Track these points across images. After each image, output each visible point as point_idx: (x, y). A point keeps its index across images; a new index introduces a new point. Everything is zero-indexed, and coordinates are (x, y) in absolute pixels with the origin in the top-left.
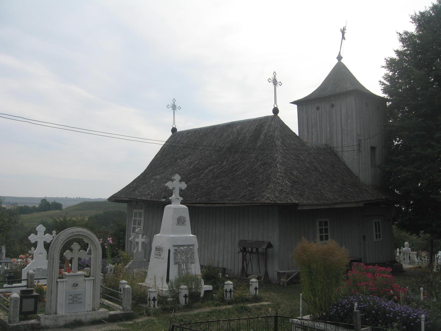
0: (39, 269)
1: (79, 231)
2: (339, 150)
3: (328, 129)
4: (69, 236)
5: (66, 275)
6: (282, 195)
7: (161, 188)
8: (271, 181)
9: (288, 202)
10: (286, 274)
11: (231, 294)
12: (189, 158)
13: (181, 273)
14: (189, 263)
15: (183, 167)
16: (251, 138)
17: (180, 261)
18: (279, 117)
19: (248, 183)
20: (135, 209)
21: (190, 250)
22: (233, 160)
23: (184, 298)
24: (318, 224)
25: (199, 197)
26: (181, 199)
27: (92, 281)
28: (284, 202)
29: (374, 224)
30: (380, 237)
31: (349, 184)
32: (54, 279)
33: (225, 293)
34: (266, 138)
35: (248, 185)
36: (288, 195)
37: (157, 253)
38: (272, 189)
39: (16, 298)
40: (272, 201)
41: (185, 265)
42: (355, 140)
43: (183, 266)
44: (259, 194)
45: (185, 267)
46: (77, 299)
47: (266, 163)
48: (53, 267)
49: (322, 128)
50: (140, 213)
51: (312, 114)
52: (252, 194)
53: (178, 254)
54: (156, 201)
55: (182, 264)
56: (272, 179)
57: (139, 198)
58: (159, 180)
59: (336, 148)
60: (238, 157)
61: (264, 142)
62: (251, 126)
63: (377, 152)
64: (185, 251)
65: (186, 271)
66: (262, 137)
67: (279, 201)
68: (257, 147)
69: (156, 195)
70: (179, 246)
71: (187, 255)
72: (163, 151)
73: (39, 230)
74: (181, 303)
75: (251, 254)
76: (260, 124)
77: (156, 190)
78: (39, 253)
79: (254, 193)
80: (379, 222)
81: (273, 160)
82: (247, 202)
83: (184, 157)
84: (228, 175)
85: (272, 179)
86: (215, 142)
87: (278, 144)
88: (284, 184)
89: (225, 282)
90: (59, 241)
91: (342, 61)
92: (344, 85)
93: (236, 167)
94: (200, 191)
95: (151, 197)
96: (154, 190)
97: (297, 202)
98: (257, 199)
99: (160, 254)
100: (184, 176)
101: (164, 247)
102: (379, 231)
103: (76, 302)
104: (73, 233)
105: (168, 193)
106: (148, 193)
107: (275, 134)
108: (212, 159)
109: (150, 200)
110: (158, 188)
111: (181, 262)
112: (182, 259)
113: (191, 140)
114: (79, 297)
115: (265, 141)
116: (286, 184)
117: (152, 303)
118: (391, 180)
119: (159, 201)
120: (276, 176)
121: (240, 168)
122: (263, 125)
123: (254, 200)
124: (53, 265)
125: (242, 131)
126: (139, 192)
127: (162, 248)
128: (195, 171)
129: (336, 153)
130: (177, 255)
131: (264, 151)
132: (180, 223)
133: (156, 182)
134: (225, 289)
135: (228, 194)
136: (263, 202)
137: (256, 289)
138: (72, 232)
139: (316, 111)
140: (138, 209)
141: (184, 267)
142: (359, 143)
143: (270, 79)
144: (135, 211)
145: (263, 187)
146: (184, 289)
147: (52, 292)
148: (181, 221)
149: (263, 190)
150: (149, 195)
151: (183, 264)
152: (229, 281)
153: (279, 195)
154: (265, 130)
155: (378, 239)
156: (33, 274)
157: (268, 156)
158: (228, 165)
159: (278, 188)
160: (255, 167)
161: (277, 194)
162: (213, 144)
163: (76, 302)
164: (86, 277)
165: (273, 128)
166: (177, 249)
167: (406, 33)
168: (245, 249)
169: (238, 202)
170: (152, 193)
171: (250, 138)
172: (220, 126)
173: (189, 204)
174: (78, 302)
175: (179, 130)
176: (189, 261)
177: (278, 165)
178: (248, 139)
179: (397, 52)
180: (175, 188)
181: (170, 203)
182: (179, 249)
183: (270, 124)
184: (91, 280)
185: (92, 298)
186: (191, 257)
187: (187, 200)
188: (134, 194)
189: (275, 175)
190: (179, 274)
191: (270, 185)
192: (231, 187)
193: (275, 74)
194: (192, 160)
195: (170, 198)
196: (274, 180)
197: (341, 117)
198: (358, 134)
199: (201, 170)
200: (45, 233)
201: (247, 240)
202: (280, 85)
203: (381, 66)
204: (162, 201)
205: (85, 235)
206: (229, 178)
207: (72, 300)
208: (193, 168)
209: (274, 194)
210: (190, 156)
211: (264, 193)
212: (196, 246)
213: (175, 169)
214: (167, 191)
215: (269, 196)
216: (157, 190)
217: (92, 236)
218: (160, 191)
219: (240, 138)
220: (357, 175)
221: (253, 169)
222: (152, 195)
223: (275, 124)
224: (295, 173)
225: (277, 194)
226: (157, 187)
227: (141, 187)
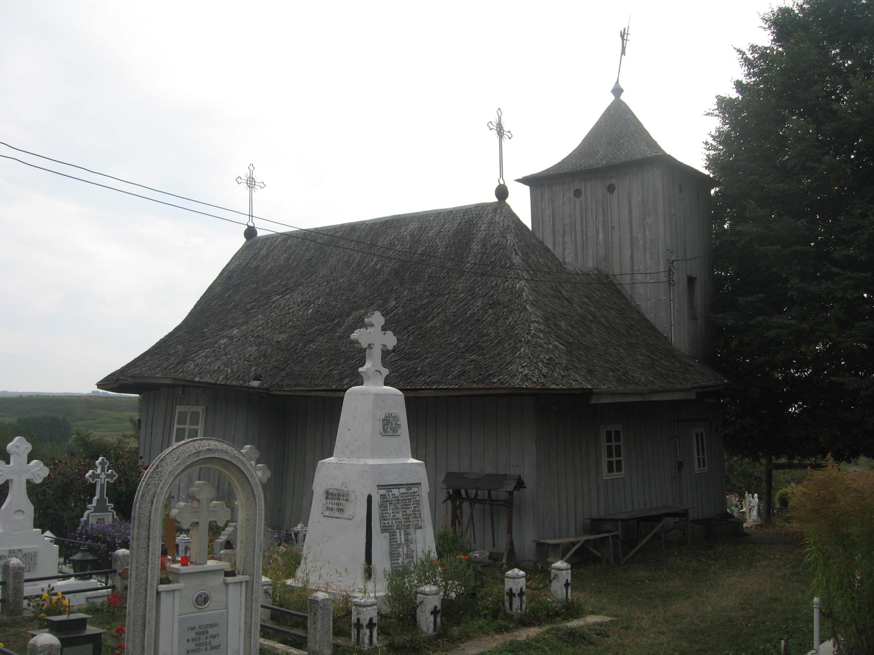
0: (15, 552)
1: (212, 450)
2: (627, 279)
3: (601, 236)
4: (188, 463)
5: (181, 572)
6: (554, 370)
7: (246, 356)
8: (520, 341)
9: (573, 387)
10: (561, 546)
11: (521, 600)
12: (301, 293)
13: (396, 554)
14: (411, 527)
15: (291, 311)
16: (449, 249)
17: (392, 523)
18: (509, 206)
19: (462, 345)
20: (180, 405)
21: (413, 496)
22: (413, 296)
23: (432, 616)
24: (603, 436)
25: (346, 377)
26: (386, 372)
27: (244, 585)
28: (563, 385)
29: (695, 436)
30: (704, 466)
31: (660, 353)
32: (152, 586)
33: (506, 597)
34: (486, 249)
35: (464, 350)
36: (569, 371)
37: (330, 506)
38: (529, 358)
39: (51, 646)
40: (537, 385)
41: (402, 533)
42: (661, 261)
43: (400, 535)
44: (502, 369)
45: (403, 537)
46: (206, 638)
47: (498, 303)
48: (148, 550)
49: (586, 234)
50: (195, 415)
51: (563, 206)
52: (481, 368)
53: (389, 508)
54: (238, 386)
55: (398, 532)
56: (523, 337)
57: (197, 379)
58: (239, 339)
59: (617, 277)
60: (424, 291)
61: (483, 257)
62: (443, 225)
63: (698, 287)
64: (402, 500)
65: (405, 547)
66: (475, 247)
67: (553, 384)
68: (467, 268)
69: (237, 372)
70: (389, 487)
71: (408, 508)
72: (228, 277)
73: (16, 450)
74: (424, 629)
75: (474, 504)
76: (465, 220)
77: (234, 361)
78: (14, 511)
79: (487, 367)
80: (702, 434)
81: (514, 296)
82: (475, 386)
83: (286, 290)
84: (406, 328)
85: (523, 337)
86: (358, 258)
87: (518, 262)
88: (551, 346)
89: (507, 573)
90: (165, 477)
91: (623, 97)
92: (634, 147)
93: (422, 312)
94: (344, 362)
95: (226, 376)
96: (231, 361)
97: (589, 387)
98: (501, 380)
99: (341, 507)
100: (296, 331)
101: (354, 491)
102: (703, 454)
103: (204, 648)
104: (199, 453)
105: (264, 368)
106: (219, 368)
107: (508, 240)
108: (358, 294)
109: (223, 383)
110: (240, 357)
111: (395, 526)
112: (397, 519)
113: (296, 254)
114: (212, 631)
115: (485, 256)
116: (556, 347)
117: (365, 634)
118: (732, 345)
119: (245, 385)
120: (529, 330)
121: (435, 314)
122: (475, 221)
123: (494, 383)
124: (148, 546)
125: (424, 235)
126: (197, 365)
127: (347, 493)
128: (322, 320)
129: (618, 287)
130: (387, 510)
131: (484, 278)
132: (389, 430)
133: (232, 342)
134: (507, 588)
135: (419, 369)
136: (517, 386)
137: (567, 585)
138: (195, 451)
139: (574, 199)
140: (188, 405)
141: (401, 537)
142: (670, 268)
143: (492, 124)
144: (179, 409)
145: (506, 355)
146: (432, 595)
147: (147, 624)
148: (390, 424)
149: (508, 361)
150: (220, 372)
151: (400, 532)
152: (515, 569)
153: (548, 370)
154: (482, 232)
155: (702, 468)
156: (20, 568)
157: (499, 288)
158: (403, 308)
159: (542, 357)
160: (471, 311)
161: (542, 368)
162: (354, 263)
163: (204, 648)
164: (111, 566)
165: (501, 229)
166: (385, 495)
167: (754, 48)
168: (457, 492)
169: (451, 387)
170: (227, 367)
171: (446, 248)
172: (367, 225)
173: (323, 393)
174: (209, 647)
175: (260, 233)
176: (411, 524)
177: (528, 307)
178: (442, 252)
179: (739, 85)
180: (373, 344)
181: (358, 380)
182: (390, 494)
183: (492, 220)
184: (241, 582)
185: (242, 633)
186: (415, 514)
187: (316, 382)
188: (185, 369)
189: (527, 328)
190: (392, 556)
191: (522, 349)
192: (423, 355)
193: (500, 114)
194: (307, 296)
195: (360, 369)
196: (528, 339)
197: (630, 213)
198: (668, 250)
199: (335, 318)
200: (30, 458)
201: (464, 473)
202: (510, 138)
203: (705, 111)
204: (253, 385)
205: (228, 458)
206: (411, 335)
207: (194, 641)
208: (315, 313)
209: (536, 368)
210: (301, 288)
211: (514, 367)
212: (425, 489)
213: (272, 316)
214: (260, 363)
215: (527, 372)
216: (237, 362)
217: (243, 463)
218: (246, 363)
219: (420, 250)
220: (665, 335)
221: (467, 315)
222: (227, 372)
223: (503, 220)
224: (563, 324)
225: (544, 368)
226: (236, 355)
227: (198, 355)
